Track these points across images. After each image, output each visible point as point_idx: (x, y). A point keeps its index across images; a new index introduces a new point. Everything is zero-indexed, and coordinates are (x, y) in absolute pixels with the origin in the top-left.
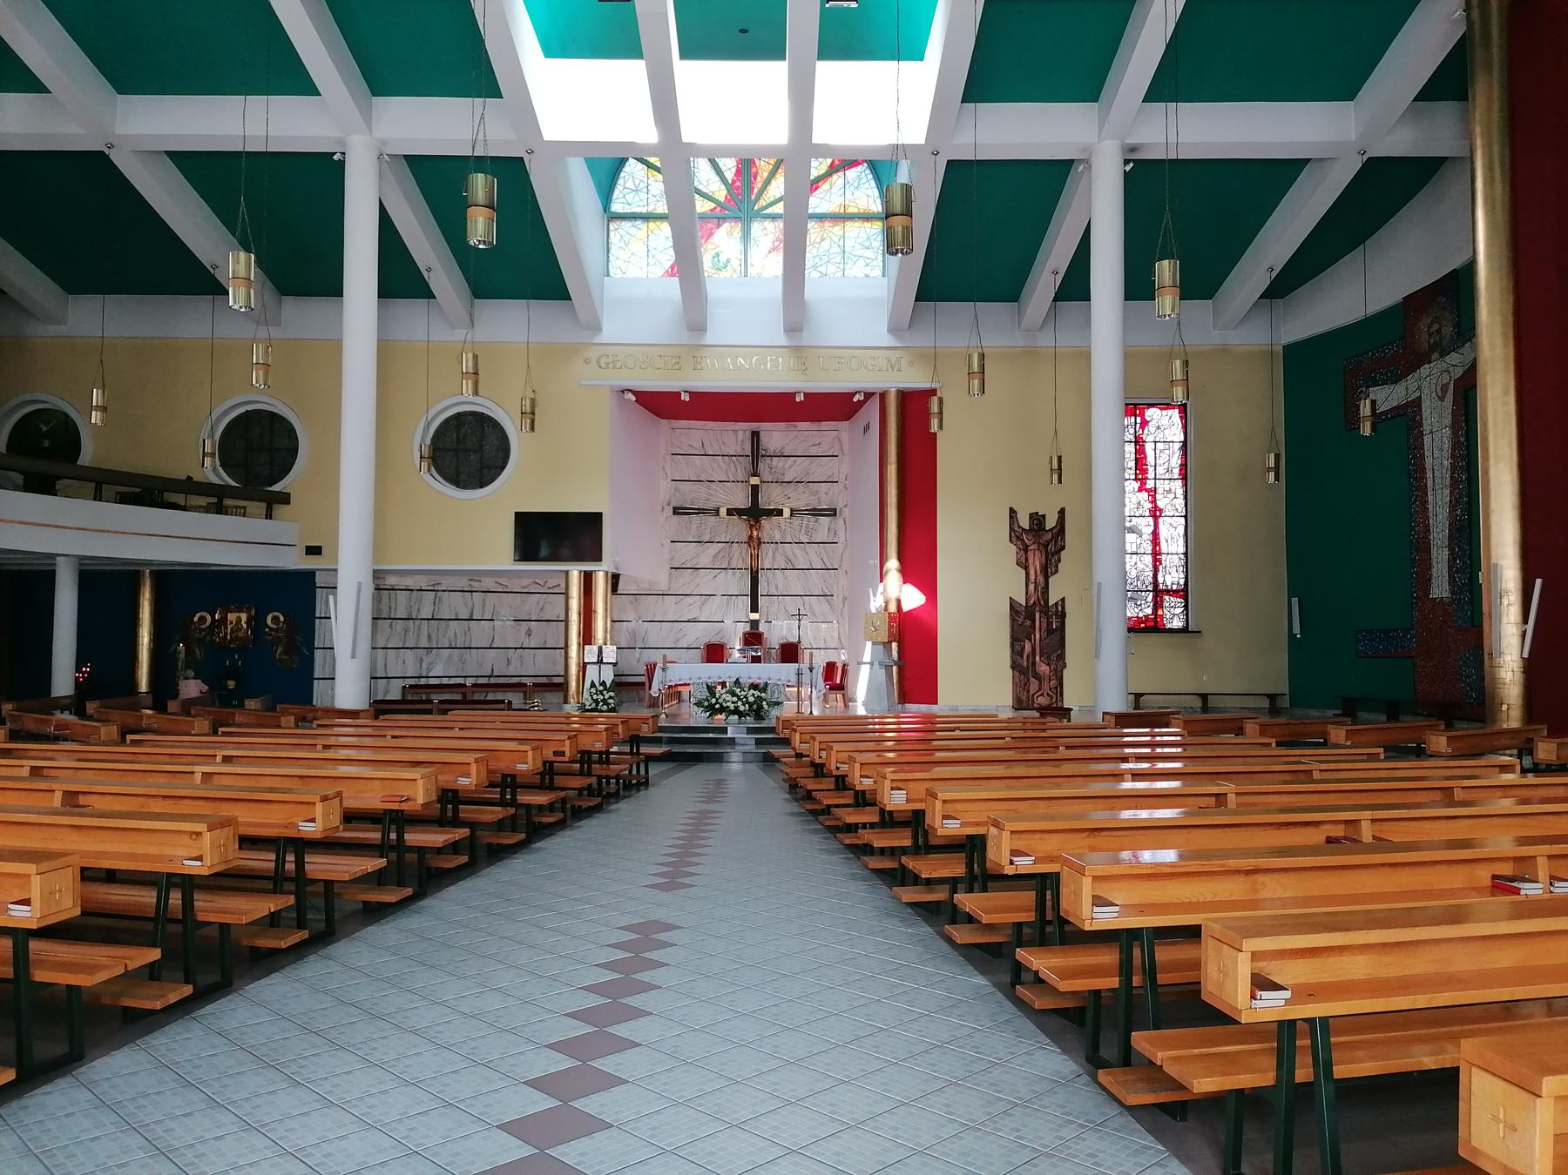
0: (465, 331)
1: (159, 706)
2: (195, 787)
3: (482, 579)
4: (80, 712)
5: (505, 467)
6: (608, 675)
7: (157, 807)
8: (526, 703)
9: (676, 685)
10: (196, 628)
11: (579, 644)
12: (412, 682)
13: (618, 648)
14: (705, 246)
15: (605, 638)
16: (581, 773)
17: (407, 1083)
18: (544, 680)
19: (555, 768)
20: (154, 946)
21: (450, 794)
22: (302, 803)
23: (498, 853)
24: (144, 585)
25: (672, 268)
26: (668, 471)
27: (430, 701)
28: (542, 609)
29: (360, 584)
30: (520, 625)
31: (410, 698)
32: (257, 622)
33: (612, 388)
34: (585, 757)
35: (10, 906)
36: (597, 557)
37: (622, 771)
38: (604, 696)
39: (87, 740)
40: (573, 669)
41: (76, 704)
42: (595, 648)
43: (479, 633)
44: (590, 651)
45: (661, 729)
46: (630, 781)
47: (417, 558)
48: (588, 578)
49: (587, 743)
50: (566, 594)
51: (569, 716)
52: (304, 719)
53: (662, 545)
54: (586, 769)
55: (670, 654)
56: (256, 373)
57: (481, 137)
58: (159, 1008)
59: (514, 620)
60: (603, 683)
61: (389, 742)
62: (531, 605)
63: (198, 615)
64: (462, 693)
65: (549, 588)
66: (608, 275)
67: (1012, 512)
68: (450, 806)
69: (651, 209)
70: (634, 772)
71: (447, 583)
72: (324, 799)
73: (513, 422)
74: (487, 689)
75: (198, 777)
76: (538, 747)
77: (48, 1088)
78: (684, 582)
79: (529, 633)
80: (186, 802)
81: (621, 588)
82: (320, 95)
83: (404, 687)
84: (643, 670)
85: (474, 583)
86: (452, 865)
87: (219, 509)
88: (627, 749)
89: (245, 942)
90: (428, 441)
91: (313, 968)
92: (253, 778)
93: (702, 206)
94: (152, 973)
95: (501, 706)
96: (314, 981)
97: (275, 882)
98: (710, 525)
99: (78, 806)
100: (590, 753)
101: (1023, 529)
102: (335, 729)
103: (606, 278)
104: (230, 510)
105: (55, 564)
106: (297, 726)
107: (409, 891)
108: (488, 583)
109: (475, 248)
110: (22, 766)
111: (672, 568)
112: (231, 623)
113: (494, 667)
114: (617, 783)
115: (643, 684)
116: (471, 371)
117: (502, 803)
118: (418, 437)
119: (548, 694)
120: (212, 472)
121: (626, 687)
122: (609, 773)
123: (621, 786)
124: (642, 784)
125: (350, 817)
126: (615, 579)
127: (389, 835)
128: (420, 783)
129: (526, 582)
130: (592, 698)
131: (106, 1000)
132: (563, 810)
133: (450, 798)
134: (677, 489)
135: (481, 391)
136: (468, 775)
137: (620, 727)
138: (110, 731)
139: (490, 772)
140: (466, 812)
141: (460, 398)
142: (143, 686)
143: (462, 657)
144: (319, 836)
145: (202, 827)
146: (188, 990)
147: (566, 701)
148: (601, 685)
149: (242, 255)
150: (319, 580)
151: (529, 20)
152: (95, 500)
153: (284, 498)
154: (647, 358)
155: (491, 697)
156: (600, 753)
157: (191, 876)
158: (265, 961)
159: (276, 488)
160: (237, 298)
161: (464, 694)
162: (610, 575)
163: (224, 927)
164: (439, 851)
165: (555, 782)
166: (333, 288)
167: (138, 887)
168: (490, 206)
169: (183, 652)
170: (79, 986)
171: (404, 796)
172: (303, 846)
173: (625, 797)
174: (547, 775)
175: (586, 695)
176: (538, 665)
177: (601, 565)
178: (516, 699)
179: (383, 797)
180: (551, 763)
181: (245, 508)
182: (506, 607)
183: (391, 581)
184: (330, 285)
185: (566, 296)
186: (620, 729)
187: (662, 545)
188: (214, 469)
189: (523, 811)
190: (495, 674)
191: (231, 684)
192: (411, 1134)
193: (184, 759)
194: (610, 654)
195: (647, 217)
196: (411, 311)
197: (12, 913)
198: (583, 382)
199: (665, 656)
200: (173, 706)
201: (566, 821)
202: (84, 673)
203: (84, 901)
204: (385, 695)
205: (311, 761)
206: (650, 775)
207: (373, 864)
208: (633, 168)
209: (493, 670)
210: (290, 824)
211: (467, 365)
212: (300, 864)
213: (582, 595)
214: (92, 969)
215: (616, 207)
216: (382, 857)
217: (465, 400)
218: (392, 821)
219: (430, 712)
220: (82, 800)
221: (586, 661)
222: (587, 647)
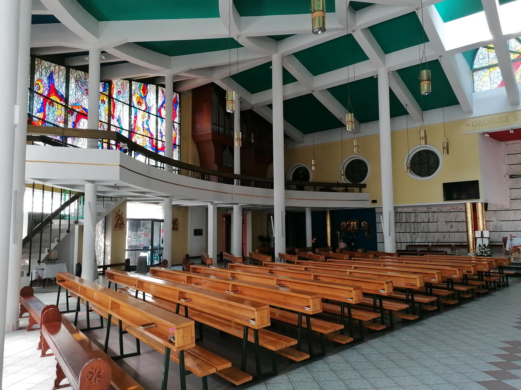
0: (421, 123)
1: (334, 251)
2: (347, 276)
3: (432, 208)
4: (314, 252)
5: (438, 168)
6: (486, 242)
7: (338, 281)
8: (452, 252)
9: (517, 246)
10: (342, 227)
11: (473, 230)
12: (410, 244)
13: (489, 232)
14: (516, 72)
15: (484, 228)
16: (479, 280)
17: (355, 369)
18: (459, 244)
19: (468, 277)
20: (341, 324)
21: (429, 284)
22: (380, 284)
23: (448, 307)
24: (328, 214)
25: (502, 83)
26: (506, 161)
27: (417, 251)
29: (390, 211)
30: (448, 223)
31: (409, 250)
32: (359, 225)
33: (478, 133)
34: (480, 274)
35: (305, 307)
36: (478, 197)
37: (496, 280)
38: (485, 250)
39: (317, 260)
40: (471, 240)
41: (313, 249)
42: (480, 232)
43: (432, 227)
44: (478, 233)
45: (513, 264)
46: (500, 284)
47: (407, 202)
48: (474, 206)
49: (480, 268)
50: (466, 212)
51: (470, 258)
52: (376, 256)
53: (506, 190)
54: (481, 278)
55: (514, 234)
56: (355, 149)
57: (424, 56)
58: (344, 343)
59: (445, 222)
60: (484, 245)
61: (404, 265)
62: (452, 216)
63: (342, 223)
64: (428, 248)
65: (458, 210)
66: (474, 92)
68: (429, 289)
69: (490, 63)
70: (502, 280)
71: (419, 210)
72: (387, 283)
73: (441, 153)
74: (437, 247)
75: (348, 273)
76: (460, 268)
77: (317, 362)
79: (452, 226)
80: (346, 280)
81: (489, 209)
83: (407, 246)
84: (501, 240)
85: (429, 209)
86: (431, 309)
87: (346, 191)
88: (498, 271)
89: (367, 327)
90: (409, 162)
91: (388, 338)
92: (364, 274)
93: (513, 57)
94: (341, 332)
95: (443, 253)
96: (389, 343)
97: (374, 309)
99: (318, 280)
100: (482, 272)
102: (386, 259)
103: (473, 93)
104: (349, 191)
105: (305, 210)
106: (374, 258)
107: (417, 317)
108: (435, 209)
109: (424, 95)
110: (302, 267)
111: (511, 199)
112: (352, 225)
113: (439, 239)
114: (495, 284)
115: (502, 245)
116: (424, 136)
117: (448, 289)
118: (405, 161)
119: (461, 249)
120: (344, 180)
121: (494, 247)
122: (491, 280)
123: (496, 286)
124: (506, 285)
125: (396, 289)
126: (486, 206)
127: (408, 297)
128: (418, 280)
129: (449, 208)
130: (480, 251)
131: (330, 339)
132: (472, 293)
133: (428, 286)
134: (511, 168)
135: (428, 143)
136: (435, 278)
137: (494, 262)
138: (322, 258)
139: (442, 277)
140: (435, 291)
141: (420, 146)
142: (329, 244)
143: (426, 236)
144: (386, 295)
145: (352, 289)
146: (352, 339)
147: (469, 252)
148: (483, 246)
149: (350, 114)
150: (377, 211)
151: (437, 12)
152: (314, 191)
153: (365, 186)
154: (493, 119)
155: (438, 250)
156: (486, 272)
157: (350, 304)
158: (374, 334)
159: (362, 183)
160: (349, 127)
161: (429, 248)
162: (483, 204)
163: (360, 321)
164: (426, 304)
165: (468, 282)
166: (376, 118)
167: (330, 304)
168: (428, 80)
169: (339, 234)
170: (323, 333)
171: (413, 284)
172: (382, 297)
173: (498, 290)
174: (465, 280)
175: (477, 249)
176: (456, 238)
177: (479, 200)
178: (449, 251)
179: (405, 284)
180: (466, 275)
181: (353, 190)
182: (442, 217)
183: (399, 210)
184: (375, 117)
185: (458, 103)
186: (494, 263)
187: (506, 190)
188: (344, 179)
189: (456, 293)
190: (439, 241)
191: (353, 244)
192: (350, 384)
193: (343, 267)
194: (486, 234)
195: (489, 67)
196: (402, 121)
197: (306, 309)
198: (466, 133)
199: (511, 235)
200: (338, 250)
201: (474, 298)
202: (314, 240)
203: (323, 308)
204: (400, 249)
205: (381, 270)
206: (509, 282)
207: (404, 306)
208: (482, 51)
209: (439, 240)
210: (377, 290)
211: (422, 134)
212: (381, 303)
213: (472, 212)
214: (326, 329)
215: (476, 66)
216: (407, 304)
217: (422, 146)
218: (409, 292)
219: (416, 254)
220: (319, 278)
221: (476, 237)
222: (476, 232)
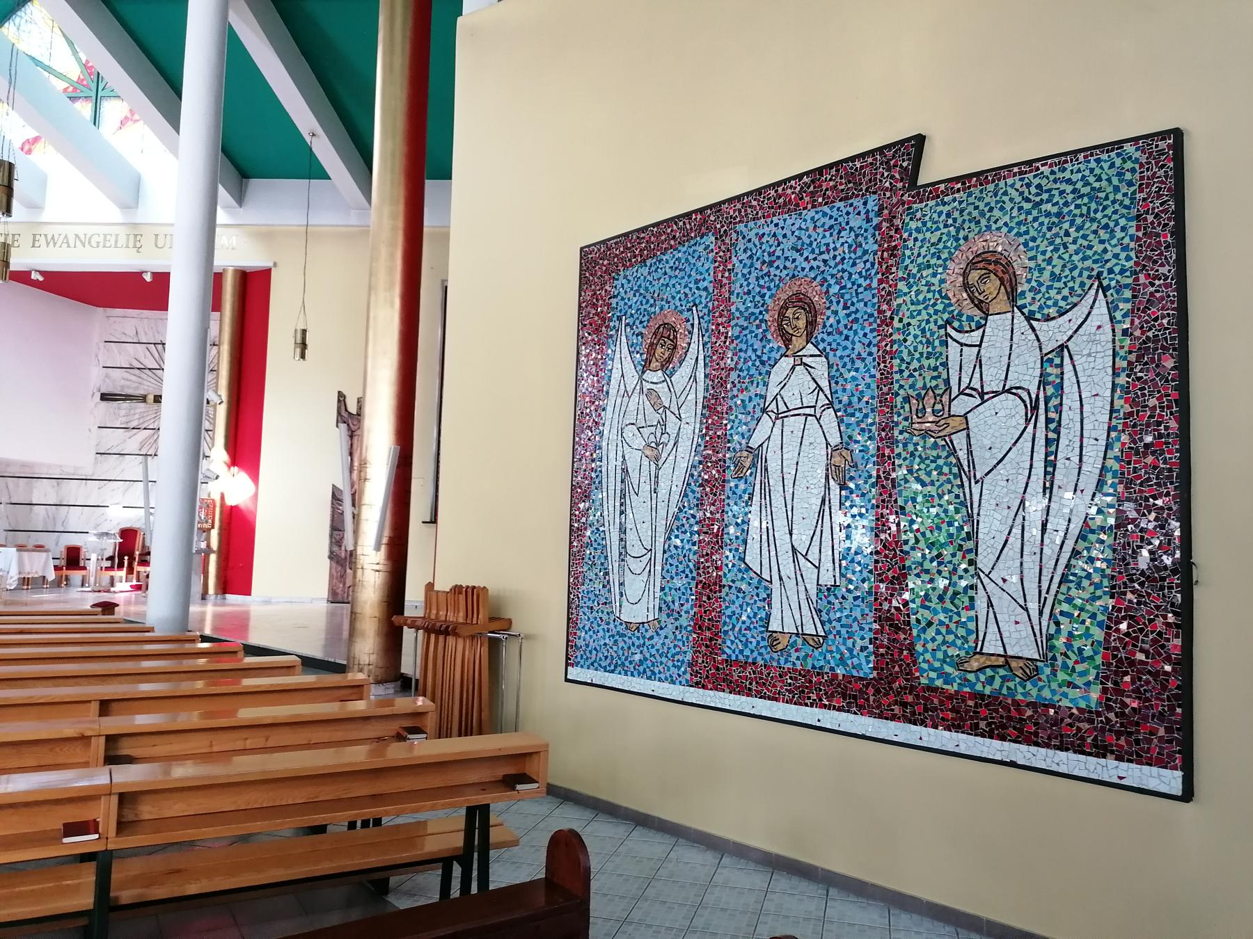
28: (45, 495)
67: (341, 397)
78: (110, 467)
82: (330, 179)
98: (138, 411)
101: (350, 413)
134: (107, 376)
